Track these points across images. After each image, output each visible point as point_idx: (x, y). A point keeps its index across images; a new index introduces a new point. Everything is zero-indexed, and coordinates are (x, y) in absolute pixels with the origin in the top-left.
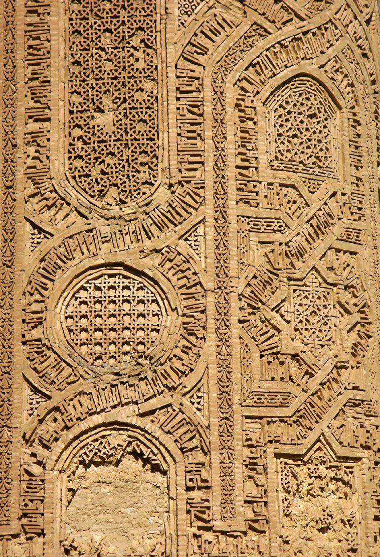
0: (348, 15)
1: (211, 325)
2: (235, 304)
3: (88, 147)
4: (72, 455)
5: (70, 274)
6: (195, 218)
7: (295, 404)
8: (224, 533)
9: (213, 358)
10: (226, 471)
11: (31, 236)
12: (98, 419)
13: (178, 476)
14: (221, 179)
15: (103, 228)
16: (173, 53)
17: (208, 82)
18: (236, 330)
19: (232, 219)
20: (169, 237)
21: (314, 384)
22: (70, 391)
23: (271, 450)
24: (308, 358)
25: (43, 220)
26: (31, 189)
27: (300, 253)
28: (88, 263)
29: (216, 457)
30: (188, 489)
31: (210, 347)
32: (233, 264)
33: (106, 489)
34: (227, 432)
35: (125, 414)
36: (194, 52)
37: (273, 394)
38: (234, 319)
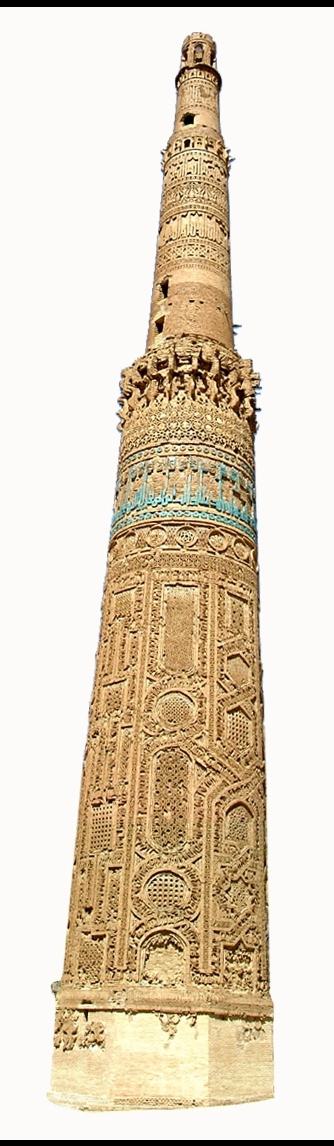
0: (256, 780)
1: (202, 895)
2: (211, 888)
3: (161, 831)
5: (151, 874)
6: (199, 855)
7: (232, 927)
8: (204, 974)
9: (203, 908)
10: (205, 950)
11: (160, 979)
12: (159, 929)
13: (187, 951)
14: (208, 842)
15: (164, 857)
16: (193, 790)
17: (206, 802)
18: (211, 898)
19: (212, 856)
20: (188, 863)
21: (239, 920)
22: (149, 918)
23: (222, 943)
25: (142, 853)
26: (138, 842)
27: (235, 872)
29: (202, 945)
31: (201, 903)
32: (211, 873)
33: (160, 955)
34: (206, 937)
36: (201, 792)
37: (224, 923)
38: (211, 894)
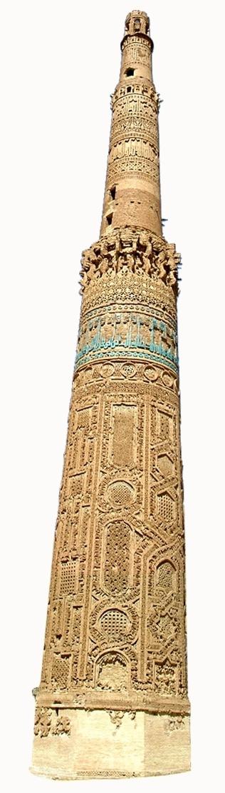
2: (146, 621)
3: (110, 580)
4: (93, 480)
6: (137, 598)
7: (161, 648)
12: (109, 650)
13: (129, 666)
14: (144, 588)
16: (133, 551)
17: (142, 560)
18: (146, 628)
20: (129, 603)
22: (102, 642)
23: (154, 661)
24: (164, 636)
25: (97, 596)
26: (94, 588)
27: (163, 609)
28: (108, 608)
29: (139, 662)
30: (132, 670)
32: (146, 611)
34: (142, 656)
35: (116, 649)
36: (139, 552)
37: (155, 646)
38: (146, 625)
